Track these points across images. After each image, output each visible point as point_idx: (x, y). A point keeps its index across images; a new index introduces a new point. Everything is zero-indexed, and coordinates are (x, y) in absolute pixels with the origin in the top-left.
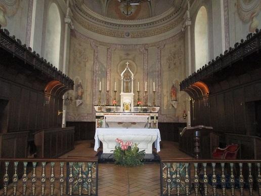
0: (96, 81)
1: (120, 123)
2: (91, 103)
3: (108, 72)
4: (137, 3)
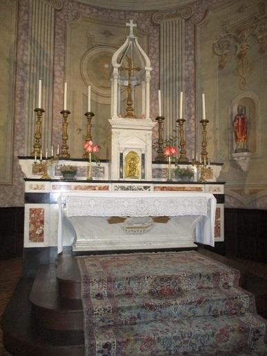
0: (22, 90)
1: (114, 220)
2: (9, 154)
3: (57, 74)
4: (37, 85)
